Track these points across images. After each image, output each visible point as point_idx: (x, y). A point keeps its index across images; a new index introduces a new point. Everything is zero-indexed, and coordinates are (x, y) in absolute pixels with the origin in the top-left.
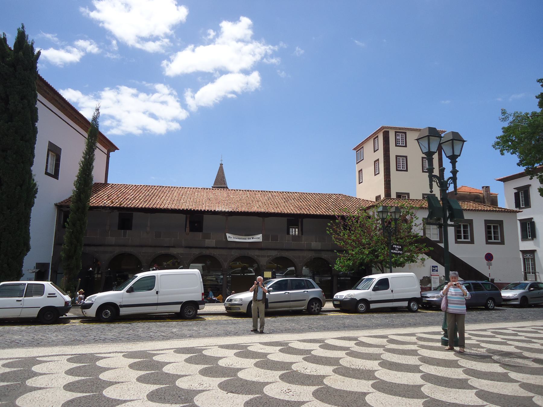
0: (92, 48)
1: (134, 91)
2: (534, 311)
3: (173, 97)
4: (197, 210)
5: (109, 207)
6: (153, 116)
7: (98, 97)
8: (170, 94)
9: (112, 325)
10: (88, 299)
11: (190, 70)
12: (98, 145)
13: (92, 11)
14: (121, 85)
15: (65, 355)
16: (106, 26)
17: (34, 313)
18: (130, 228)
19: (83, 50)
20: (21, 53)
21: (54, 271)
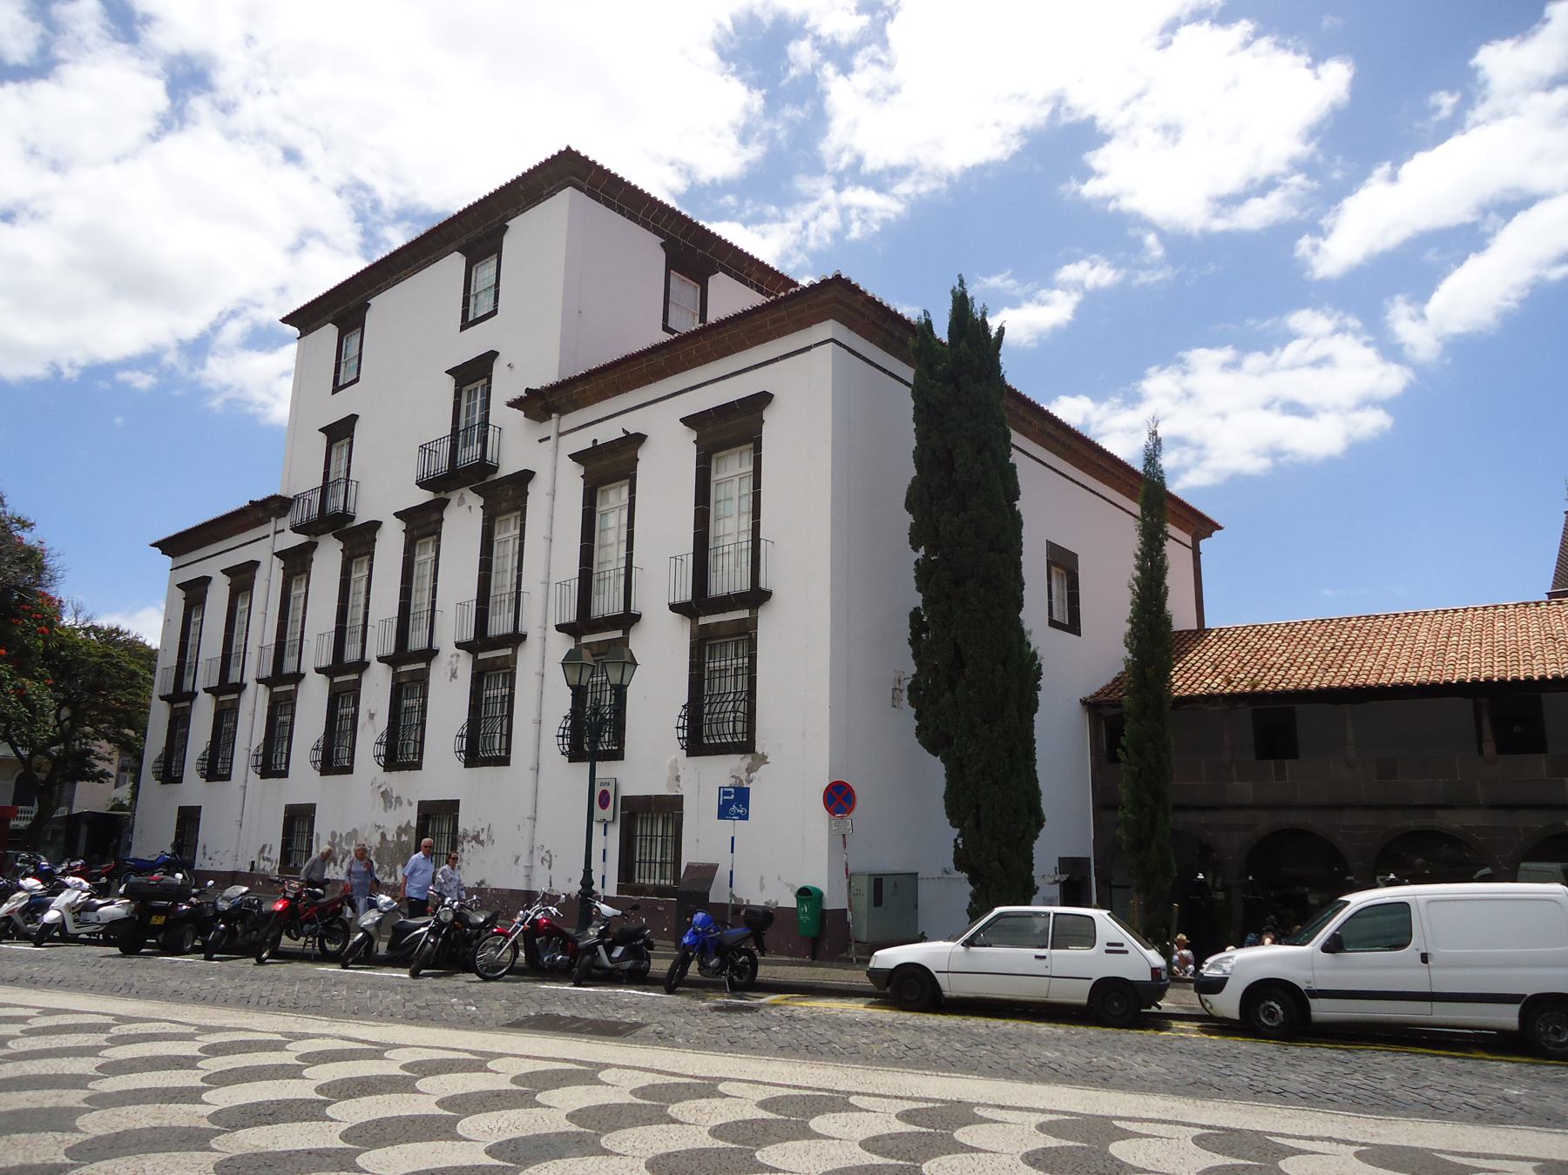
0: (1096, 274)
1: (1226, 354)
2: (941, 1032)
3: (1349, 338)
4: (1516, 680)
5: (1221, 695)
6: (1294, 408)
7: (1133, 399)
8: (1340, 330)
9: (1296, 1051)
10: (1213, 966)
11: (1394, 238)
12: (1172, 529)
13: (1085, 182)
14: (1188, 347)
15: (1184, 1124)
16: (1127, 204)
17: (1079, 994)
18: (1293, 754)
19: (1078, 285)
20: (963, 344)
21: (1103, 882)
